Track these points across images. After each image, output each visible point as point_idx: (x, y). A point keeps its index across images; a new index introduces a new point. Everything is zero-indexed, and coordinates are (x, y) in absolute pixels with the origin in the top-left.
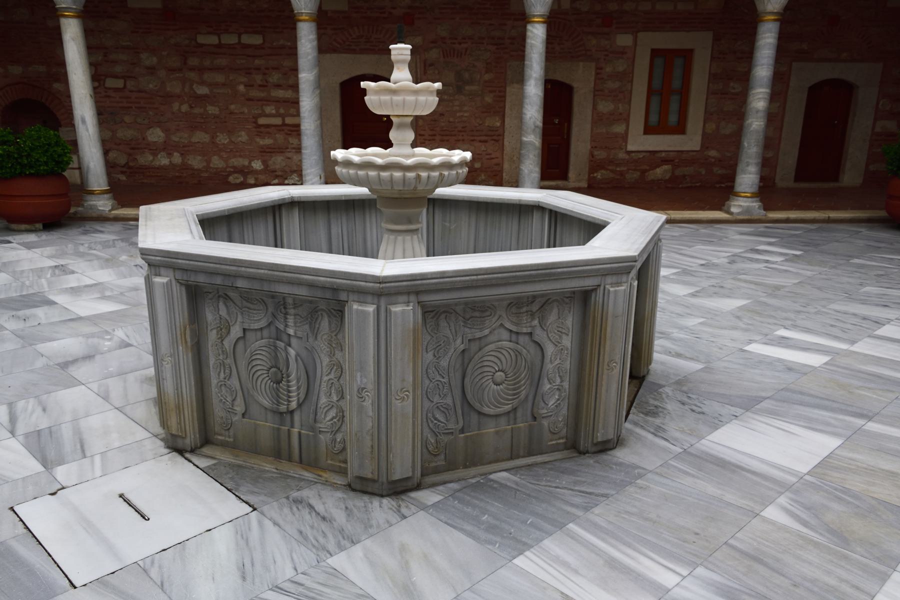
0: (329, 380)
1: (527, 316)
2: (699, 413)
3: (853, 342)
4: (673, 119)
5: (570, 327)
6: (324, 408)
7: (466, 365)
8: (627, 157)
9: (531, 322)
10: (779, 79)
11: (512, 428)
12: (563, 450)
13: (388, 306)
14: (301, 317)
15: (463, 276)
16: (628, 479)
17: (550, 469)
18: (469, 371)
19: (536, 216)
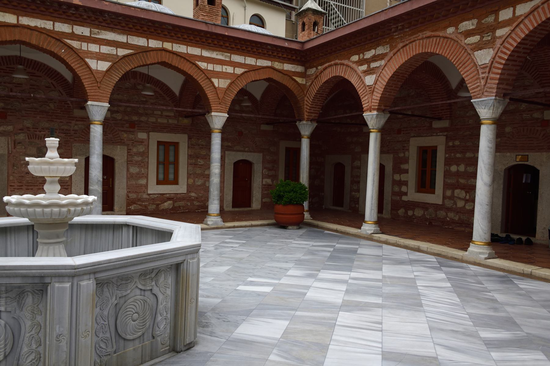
0: (31, 335)
1: (149, 280)
2: (228, 322)
3: (280, 279)
4: (171, 177)
5: (170, 284)
6: (25, 355)
7: (117, 312)
8: (148, 197)
9: (151, 283)
10: (223, 158)
11: (142, 345)
12: (168, 353)
13: (79, 282)
14: (11, 298)
15: (120, 261)
16: (206, 359)
17: (165, 364)
18: (119, 315)
19: (125, 230)
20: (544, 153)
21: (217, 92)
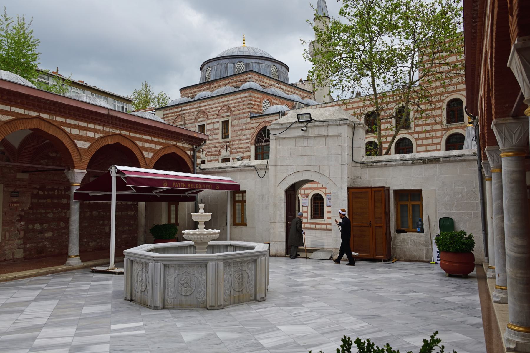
21: (146, 163)
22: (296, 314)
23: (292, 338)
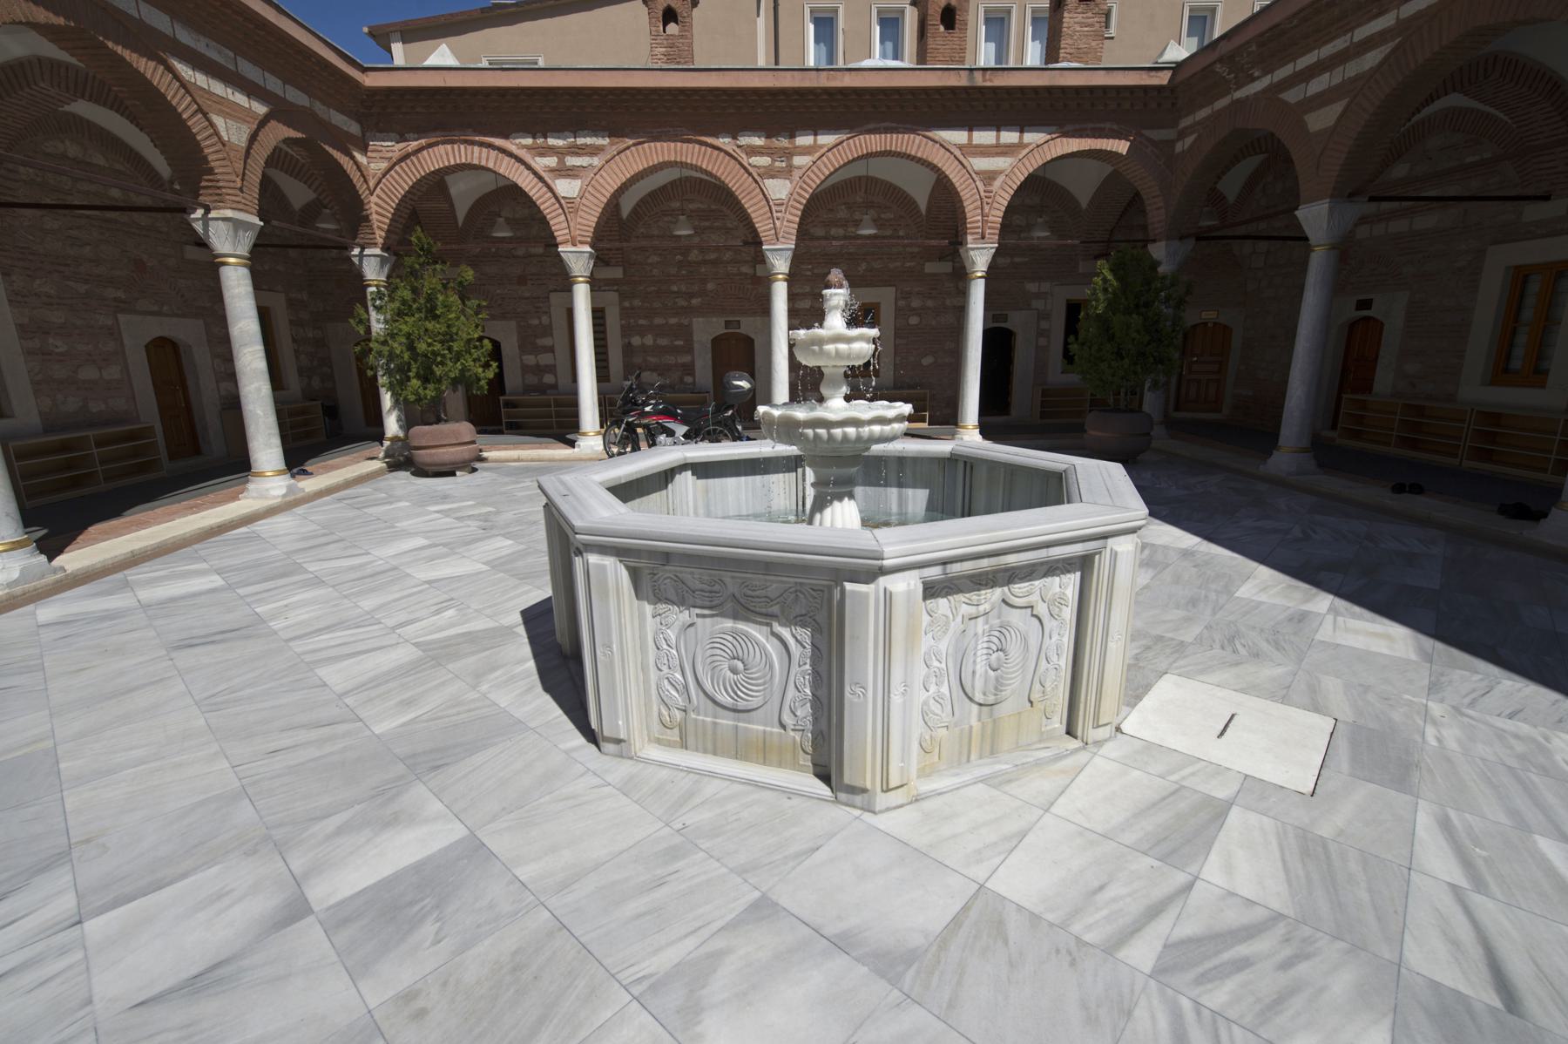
20: (758, 318)
22: (447, 608)
23: (457, 553)
